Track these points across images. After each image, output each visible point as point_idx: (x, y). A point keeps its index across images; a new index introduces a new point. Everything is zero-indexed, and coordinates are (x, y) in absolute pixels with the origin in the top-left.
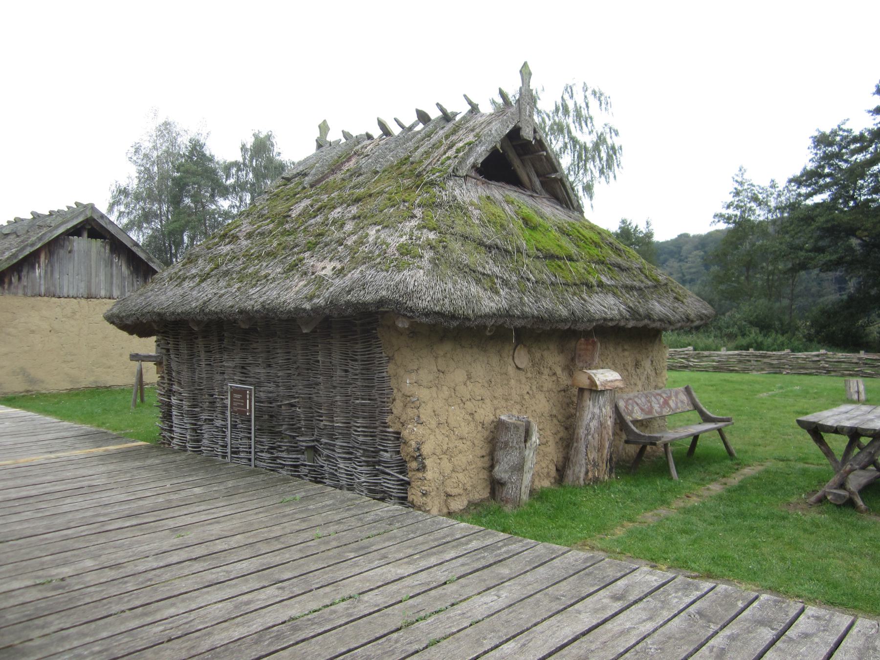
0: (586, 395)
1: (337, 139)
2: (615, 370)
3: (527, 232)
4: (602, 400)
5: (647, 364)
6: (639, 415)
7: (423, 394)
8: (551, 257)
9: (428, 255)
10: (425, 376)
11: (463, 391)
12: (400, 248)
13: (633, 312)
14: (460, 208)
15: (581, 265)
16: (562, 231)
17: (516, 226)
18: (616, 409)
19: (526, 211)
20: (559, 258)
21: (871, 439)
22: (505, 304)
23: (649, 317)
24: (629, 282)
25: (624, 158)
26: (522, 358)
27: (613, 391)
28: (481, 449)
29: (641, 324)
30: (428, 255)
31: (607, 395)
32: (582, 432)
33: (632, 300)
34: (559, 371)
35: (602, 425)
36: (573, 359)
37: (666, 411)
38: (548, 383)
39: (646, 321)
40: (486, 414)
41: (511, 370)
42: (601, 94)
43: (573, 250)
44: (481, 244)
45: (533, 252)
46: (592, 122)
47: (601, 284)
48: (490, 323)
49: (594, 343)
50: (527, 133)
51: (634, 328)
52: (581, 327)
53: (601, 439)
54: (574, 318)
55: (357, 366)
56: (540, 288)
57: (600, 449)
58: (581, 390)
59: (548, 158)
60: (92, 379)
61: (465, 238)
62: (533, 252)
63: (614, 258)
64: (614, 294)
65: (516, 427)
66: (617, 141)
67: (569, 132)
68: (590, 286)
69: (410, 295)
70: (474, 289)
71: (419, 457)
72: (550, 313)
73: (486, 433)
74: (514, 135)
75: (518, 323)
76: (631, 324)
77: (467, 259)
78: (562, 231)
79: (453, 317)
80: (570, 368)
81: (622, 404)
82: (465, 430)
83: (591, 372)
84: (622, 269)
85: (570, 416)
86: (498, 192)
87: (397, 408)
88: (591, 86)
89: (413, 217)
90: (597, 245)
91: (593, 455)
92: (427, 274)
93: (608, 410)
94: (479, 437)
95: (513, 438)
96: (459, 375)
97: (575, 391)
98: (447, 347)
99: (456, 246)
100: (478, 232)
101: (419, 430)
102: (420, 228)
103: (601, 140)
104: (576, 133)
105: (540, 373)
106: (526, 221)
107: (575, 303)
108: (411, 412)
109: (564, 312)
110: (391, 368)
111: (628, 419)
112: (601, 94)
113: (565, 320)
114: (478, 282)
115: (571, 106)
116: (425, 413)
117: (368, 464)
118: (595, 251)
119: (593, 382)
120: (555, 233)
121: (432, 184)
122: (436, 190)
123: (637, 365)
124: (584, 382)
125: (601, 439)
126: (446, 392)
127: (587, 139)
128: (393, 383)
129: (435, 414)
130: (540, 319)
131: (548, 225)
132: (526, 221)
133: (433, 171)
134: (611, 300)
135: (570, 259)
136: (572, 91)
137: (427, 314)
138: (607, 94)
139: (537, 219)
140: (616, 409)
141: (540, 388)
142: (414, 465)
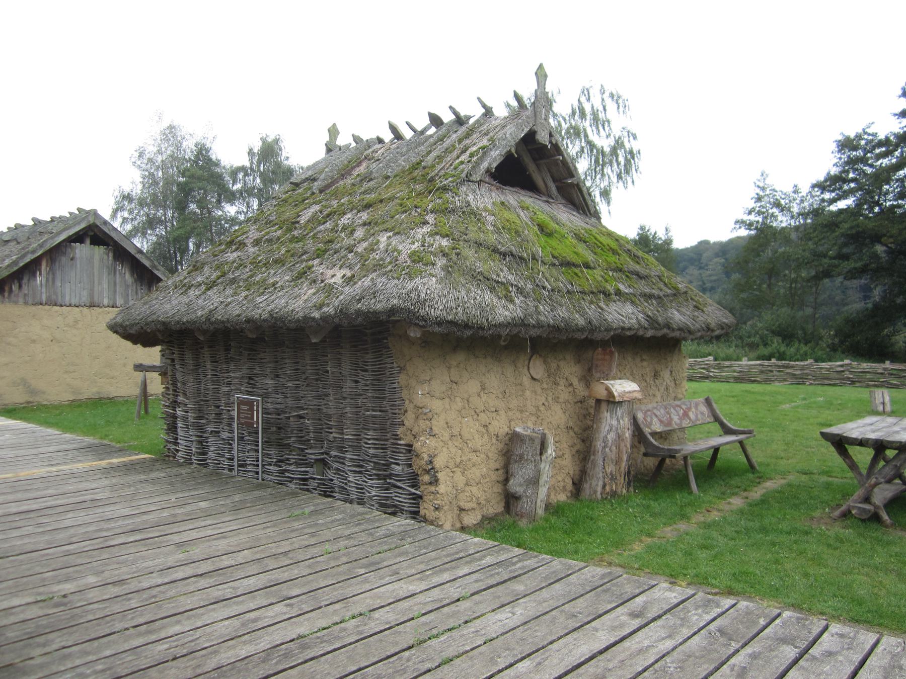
0: (604, 406)
1: (347, 143)
2: (634, 380)
3: (543, 239)
4: (619, 411)
5: (666, 374)
6: (658, 427)
7: (436, 405)
8: (568, 264)
9: (441, 262)
10: (437, 386)
11: (477, 402)
12: (412, 255)
13: (652, 321)
14: (474, 214)
15: (598, 273)
16: (579, 238)
17: (531, 233)
18: (635, 421)
19: (542, 217)
20: (576, 266)
21: (897, 452)
22: (519, 313)
23: (668, 326)
24: (647, 290)
25: (642, 162)
26: (538, 368)
27: (631, 402)
28: (496, 462)
29: (659, 334)
30: (441, 262)
31: (625, 406)
32: (599, 444)
33: (651, 308)
34: (575, 382)
35: (619, 437)
36: (590, 370)
37: (685, 423)
38: (564, 394)
39: (665, 331)
40: (500, 426)
41: (526, 380)
42: (619, 97)
43: (590, 257)
44: (495, 251)
45: (549, 259)
46: (609, 125)
47: (618, 293)
48: (505, 332)
49: (612, 353)
50: (543, 137)
51: (653, 337)
52: (598, 336)
53: (619, 452)
54: (591, 328)
55: (368, 377)
56: (556, 296)
57: (618, 462)
58: (599, 401)
59: (564, 163)
60: (95, 390)
61: (479, 244)
62: (549, 259)
63: (632, 266)
64: (633, 303)
65: (532, 439)
66: (635, 146)
67: (586, 136)
68: (607, 295)
69: (422, 303)
70: (488, 297)
71: (431, 470)
72: (567, 322)
73: (500, 446)
74: (530, 138)
75: (534, 332)
76: (650, 334)
77: (480, 267)
78: (579, 238)
79: (466, 326)
80: (587, 379)
81: (640, 416)
82: (479, 442)
83: (609, 383)
84: (640, 277)
85: (587, 428)
86: (513, 197)
87: (409, 419)
88: (609, 89)
89: (425, 223)
90: (614, 252)
91: (610, 468)
92: (439, 282)
93: (626, 422)
94: (493, 449)
95: (529, 451)
96: (473, 386)
97: (592, 402)
98: (461, 357)
99: (469, 253)
100: (492, 239)
101: (431, 442)
102: (432, 234)
103: (619, 144)
104: (593, 137)
105: (556, 384)
106: (542, 228)
107: (592, 312)
108: (423, 424)
109: (581, 321)
110: (402, 379)
111: (647, 431)
112: (619, 97)
113: (581, 330)
114: (492, 290)
115: (588, 110)
116: (438, 425)
117: (379, 477)
118: (612, 259)
119: (610, 393)
120: (571, 240)
121: (445, 189)
122: (448, 196)
123: (656, 375)
124: (601, 393)
125: (619, 452)
126: (459, 403)
127: (604, 143)
128: (405, 394)
129: (448, 425)
130: (556, 329)
131: (564, 231)
132: (542, 228)
133: (445, 176)
134: (629, 309)
135: (587, 266)
136: (588, 93)
137: (440, 323)
138: (625, 97)
139: (553, 225)
140: (635, 421)
141: (556, 399)
142: (426, 478)
